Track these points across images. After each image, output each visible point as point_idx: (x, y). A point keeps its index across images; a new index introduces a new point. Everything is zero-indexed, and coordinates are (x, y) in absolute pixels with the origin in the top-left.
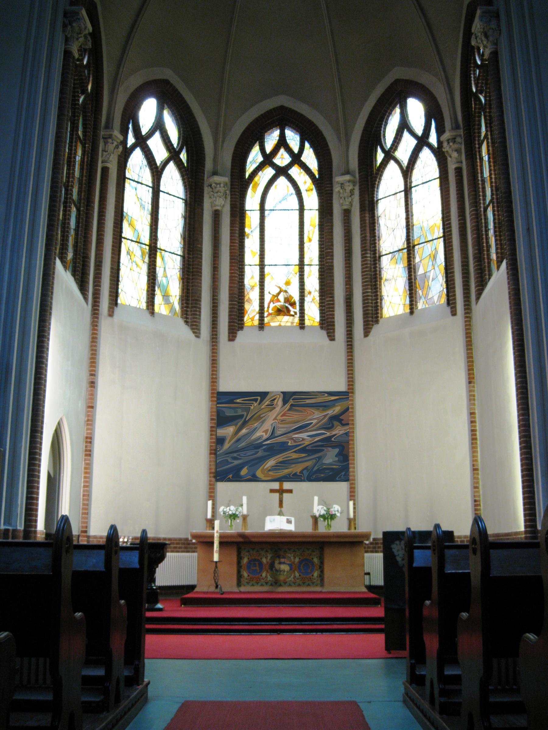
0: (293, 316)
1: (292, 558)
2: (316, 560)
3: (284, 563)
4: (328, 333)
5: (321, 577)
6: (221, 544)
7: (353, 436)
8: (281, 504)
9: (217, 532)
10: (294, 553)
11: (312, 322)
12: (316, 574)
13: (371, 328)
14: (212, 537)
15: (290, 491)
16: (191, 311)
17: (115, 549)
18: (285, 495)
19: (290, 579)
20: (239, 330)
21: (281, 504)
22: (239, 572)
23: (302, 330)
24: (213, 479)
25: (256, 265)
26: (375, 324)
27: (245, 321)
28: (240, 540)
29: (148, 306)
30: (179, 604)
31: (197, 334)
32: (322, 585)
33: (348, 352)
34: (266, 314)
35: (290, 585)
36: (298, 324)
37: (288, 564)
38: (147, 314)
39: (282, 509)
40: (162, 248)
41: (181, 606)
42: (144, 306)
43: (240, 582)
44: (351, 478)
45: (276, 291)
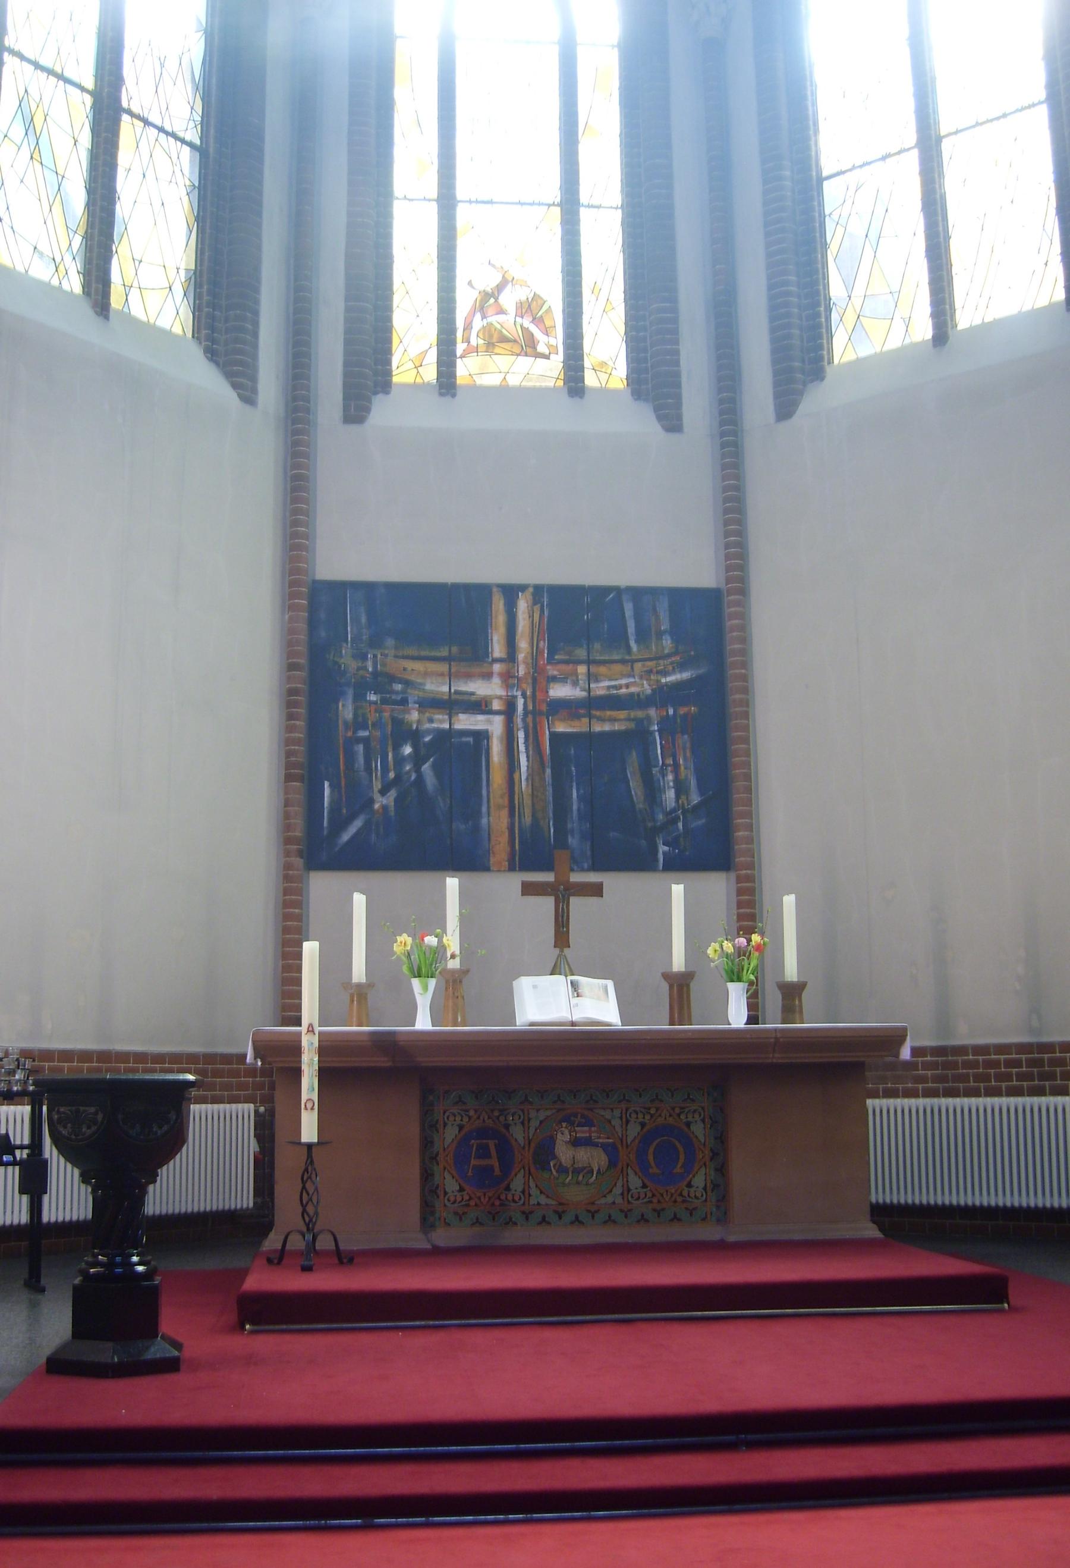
0: (547, 357)
1: (616, 1122)
2: (698, 1130)
3: (587, 1142)
4: (656, 410)
5: (720, 1189)
6: (324, 1074)
7: (746, 728)
8: (562, 938)
9: (311, 1030)
10: (623, 1105)
11: (603, 377)
12: (699, 1181)
13: (801, 393)
14: (295, 1049)
15: (597, 890)
16: (227, 320)
17: (159, 1132)
18: (576, 903)
19: (610, 1199)
20: (376, 393)
21: (562, 938)
22: (426, 1176)
23: (577, 399)
24: (299, 862)
25: (429, 200)
26: (812, 381)
27: (394, 364)
28: (383, 1061)
29: (86, 286)
30: (233, 1317)
31: (248, 394)
32: (723, 1218)
33: (724, 467)
34: (460, 348)
35: (610, 1220)
36: (560, 383)
37: (604, 1147)
38: (86, 310)
39: (566, 951)
40: (136, 109)
41: (243, 1328)
42: (74, 284)
43: (433, 1213)
44: (740, 859)
45: (489, 281)
